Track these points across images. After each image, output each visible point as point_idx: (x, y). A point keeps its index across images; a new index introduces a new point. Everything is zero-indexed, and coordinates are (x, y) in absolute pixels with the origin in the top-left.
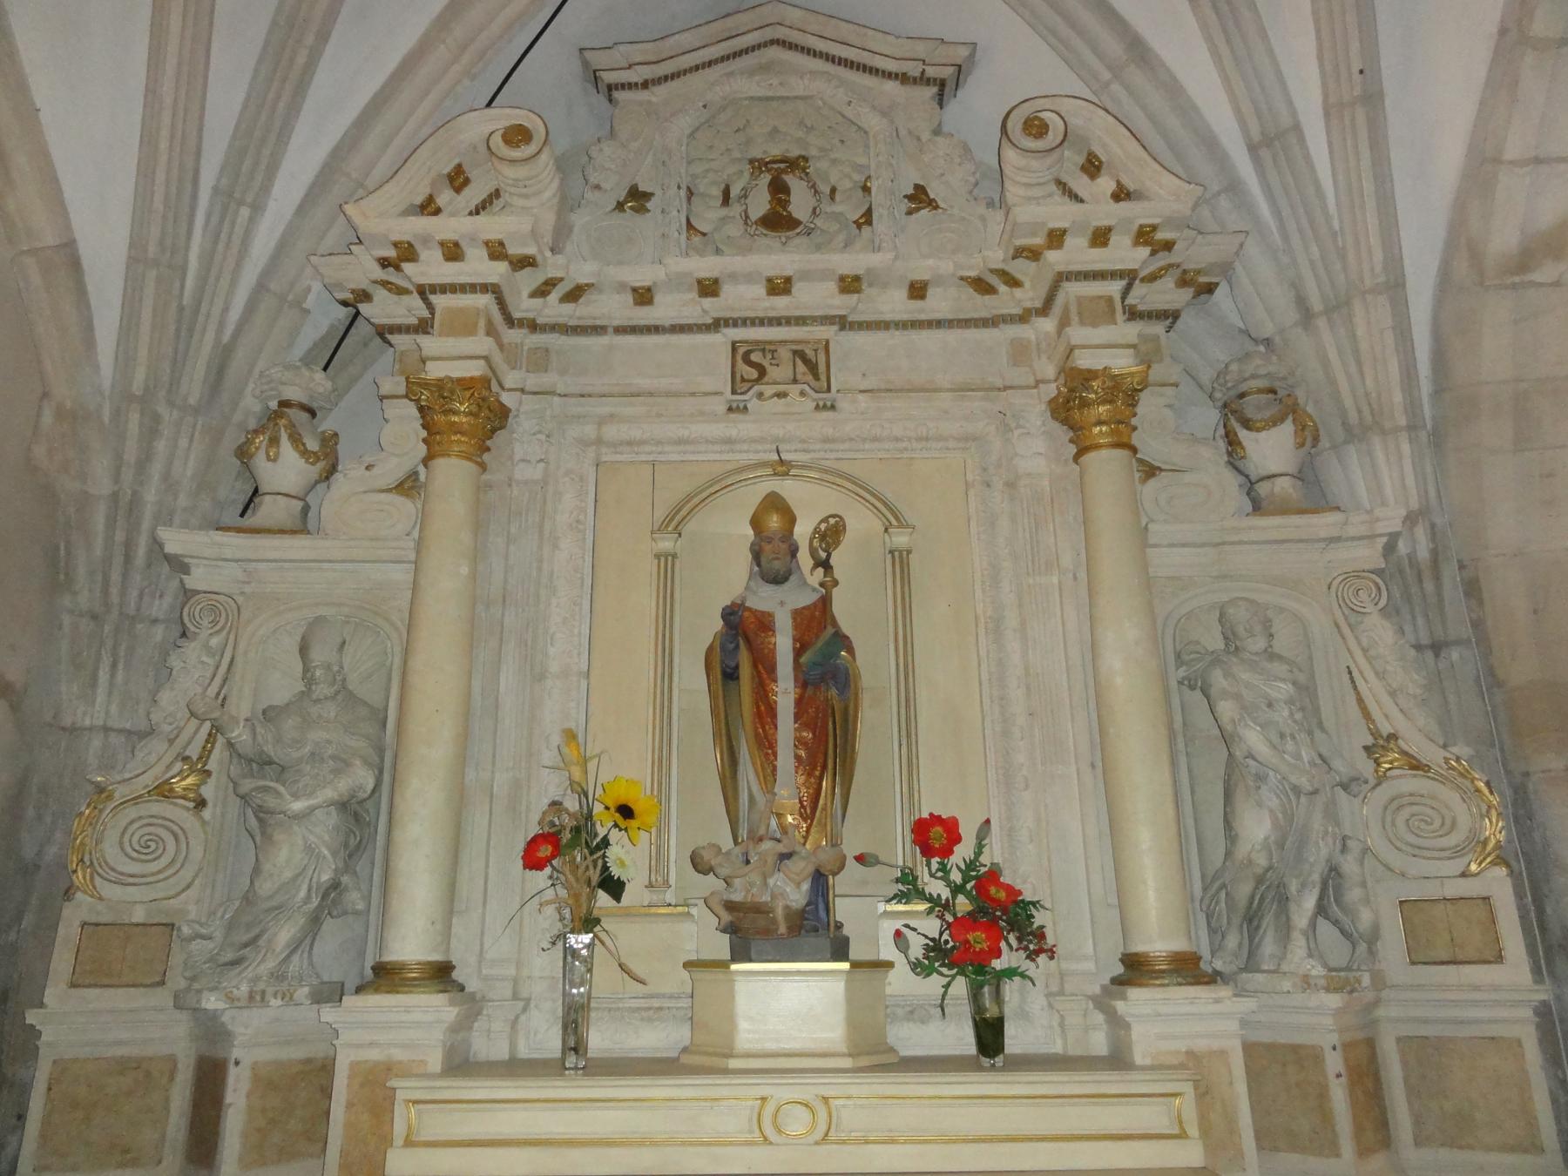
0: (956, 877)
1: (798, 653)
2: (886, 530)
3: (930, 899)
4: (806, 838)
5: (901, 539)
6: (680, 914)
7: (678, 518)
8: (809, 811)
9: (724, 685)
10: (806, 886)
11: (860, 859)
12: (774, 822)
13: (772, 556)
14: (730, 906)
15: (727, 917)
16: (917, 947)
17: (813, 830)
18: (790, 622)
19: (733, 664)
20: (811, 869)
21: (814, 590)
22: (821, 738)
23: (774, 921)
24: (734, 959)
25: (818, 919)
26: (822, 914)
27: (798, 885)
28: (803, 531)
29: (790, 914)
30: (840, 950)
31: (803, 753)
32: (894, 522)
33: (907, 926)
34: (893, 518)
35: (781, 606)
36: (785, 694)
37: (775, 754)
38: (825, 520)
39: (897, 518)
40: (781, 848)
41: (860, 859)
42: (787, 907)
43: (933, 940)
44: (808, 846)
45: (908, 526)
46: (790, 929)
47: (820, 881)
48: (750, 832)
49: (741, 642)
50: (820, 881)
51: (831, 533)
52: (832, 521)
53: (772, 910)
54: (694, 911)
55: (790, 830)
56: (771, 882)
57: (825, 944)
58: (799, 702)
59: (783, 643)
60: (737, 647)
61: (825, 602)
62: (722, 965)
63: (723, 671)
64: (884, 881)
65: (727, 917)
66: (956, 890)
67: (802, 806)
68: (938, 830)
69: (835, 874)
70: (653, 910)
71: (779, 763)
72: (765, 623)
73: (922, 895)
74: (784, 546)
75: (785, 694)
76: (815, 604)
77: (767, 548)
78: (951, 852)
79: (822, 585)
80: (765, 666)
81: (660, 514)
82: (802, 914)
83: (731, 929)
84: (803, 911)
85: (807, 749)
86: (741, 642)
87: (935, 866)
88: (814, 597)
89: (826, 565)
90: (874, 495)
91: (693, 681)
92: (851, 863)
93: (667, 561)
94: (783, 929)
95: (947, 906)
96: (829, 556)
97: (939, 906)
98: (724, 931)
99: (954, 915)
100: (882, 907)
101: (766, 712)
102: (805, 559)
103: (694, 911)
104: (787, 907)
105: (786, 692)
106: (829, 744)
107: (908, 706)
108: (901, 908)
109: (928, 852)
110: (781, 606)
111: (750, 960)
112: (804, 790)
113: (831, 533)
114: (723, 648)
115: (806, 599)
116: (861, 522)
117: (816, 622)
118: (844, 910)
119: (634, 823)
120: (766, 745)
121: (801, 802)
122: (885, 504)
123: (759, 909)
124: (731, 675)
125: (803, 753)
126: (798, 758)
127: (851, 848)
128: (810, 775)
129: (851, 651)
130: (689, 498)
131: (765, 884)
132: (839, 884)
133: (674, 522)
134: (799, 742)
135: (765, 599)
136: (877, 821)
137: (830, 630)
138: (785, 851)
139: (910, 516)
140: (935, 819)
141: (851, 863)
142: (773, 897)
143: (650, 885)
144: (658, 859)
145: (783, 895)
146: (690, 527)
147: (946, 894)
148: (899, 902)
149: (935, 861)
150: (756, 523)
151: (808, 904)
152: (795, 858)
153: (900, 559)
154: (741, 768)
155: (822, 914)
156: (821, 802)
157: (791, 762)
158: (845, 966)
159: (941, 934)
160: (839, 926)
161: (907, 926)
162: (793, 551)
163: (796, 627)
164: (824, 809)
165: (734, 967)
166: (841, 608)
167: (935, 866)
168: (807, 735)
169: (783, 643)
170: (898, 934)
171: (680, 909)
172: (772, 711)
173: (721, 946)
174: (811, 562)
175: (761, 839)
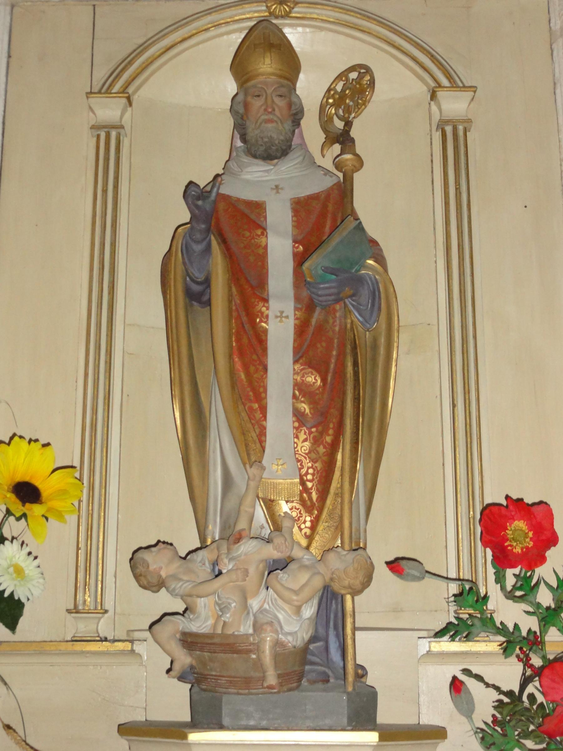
0: (545, 598)
1: (300, 260)
2: (433, 96)
3: (502, 630)
4: (310, 538)
5: (454, 105)
6: (122, 653)
7: (126, 76)
8: (315, 502)
9: (302, 691)
10: (309, 611)
11: (395, 565)
12: (260, 514)
13: (263, 121)
14: (189, 641)
15: (184, 659)
16: (484, 702)
17: (320, 528)
18: (289, 214)
19: (201, 277)
20: (318, 583)
21: (327, 172)
22: (335, 388)
23: (259, 665)
24: (196, 724)
25: (328, 662)
26: (335, 655)
27: (298, 610)
28: (311, 88)
29: (281, 653)
30: (362, 713)
31: (305, 407)
32: (445, 82)
33: (467, 672)
34: (442, 76)
35: (275, 190)
36: (280, 325)
37: (263, 410)
38: (339, 77)
39: (449, 77)
40: (272, 552)
41: (395, 565)
42: (277, 643)
43: (510, 694)
44: (312, 550)
45: (465, 88)
46: (284, 678)
47: (332, 607)
48: (223, 529)
49: (214, 243)
50: (332, 607)
51: (354, 89)
52: (353, 75)
53: (258, 648)
54: (139, 648)
55: (286, 524)
56: (255, 604)
57: (340, 701)
58: (301, 330)
59: (279, 248)
60: (208, 249)
61: (343, 193)
62: (175, 731)
63: (187, 292)
64: (436, 602)
65: (184, 659)
66: (547, 617)
67: (306, 489)
68: (519, 526)
69: (355, 592)
70: (79, 647)
71: (271, 423)
72: (249, 216)
73: (489, 624)
74: (281, 103)
75: (280, 325)
76: (328, 193)
77: (257, 104)
78: (542, 560)
79: (338, 166)
80: (249, 283)
81: (101, 74)
82: (303, 654)
83: (195, 677)
84: (305, 650)
85: (313, 403)
86: (214, 243)
87: (510, 581)
88: (327, 183)
89: (344, 139)
90: (417, 46)
91: (143, 308)
92: (382, 573)
93: (108, 142)
94: (272, 679)
95: (535, 641)
96: (348, 124)
97: (517, 643)
98: (182, 678)
99: (544, 658)
100: (424, 646)
101: (250, 345)
102: (312, 132)
103: (139, 648)
104: (277, 643)
105: (281, 316)
106: (346, 400)
107: (465, 352)
108: (456, 646)
109: (503, 559)
110: (275, 190)
111: (221, 727)
112: (307, 463)
113: (354, 89)
114: (187, 250)
115: (317, 185)
116: (396, 83)
117: (327, 216)
118: (369, 649)
119: (37, 510)
120: (249, 397)
121: (303, 483)
122: (433, 58)
123: (230, 646)
124: (198, 296)
125: (305, 407)
126: (298, 415)
127: (380, 552)
128: (316, 441)
129: (380, 259)
130: (142, 48)
131: (245, 607)
132: (363, 608)
133: (121, 81)
134: (302, 389)
135: (255, 181)
136: (418, 506)
137: (350, 224)
138: (276, 555)
139: (466, 76)
140: (518, 506)
141: (382, 573)
142: (257, 627)
143: (75, 610)
144: (87, 565)
145: (275, 624)
146: (148, 91)
147: (529, 624)
148: (452, 638)
149: (510, 574)
150: (240, 66)
151: (314, 639)
152: (292, 566)
153: (454, 138)
154: (213, 434)
155: (335, 655)
156: (335, 484)
157: (289, 421)
158: (372, 737)
159: (523, 686)
160: (361, 673)
161: (467, 672)
162: (296, 116)
163: (298, 224)
164: (340, 494)
165: (194, 737)
166: (370, 205)
167: (510, 581)
168: (313, 379)
169: (279, 248)
170: (456, 685)
171: (120, 646)
172: (260, 340)
173: (174, 701)
174: (322, 137)
175: (238, 539)
